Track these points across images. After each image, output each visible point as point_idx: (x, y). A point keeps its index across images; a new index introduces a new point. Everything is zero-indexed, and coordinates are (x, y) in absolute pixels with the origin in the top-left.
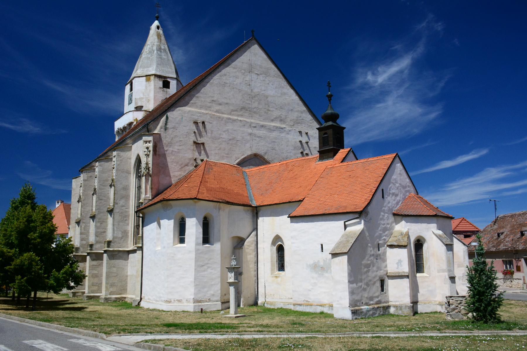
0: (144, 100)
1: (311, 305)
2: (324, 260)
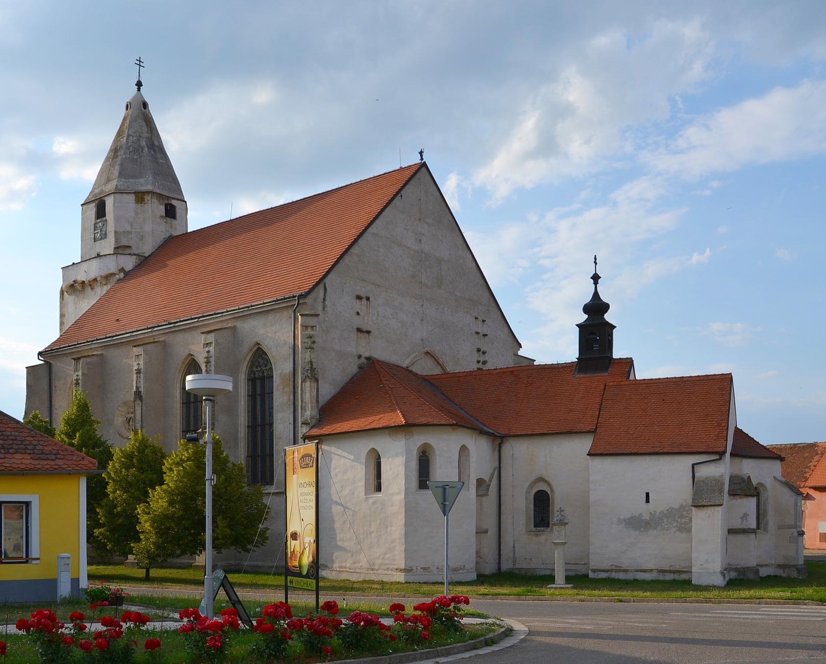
0: (133, 235)
1: (626, 571)
2: (651, 514)
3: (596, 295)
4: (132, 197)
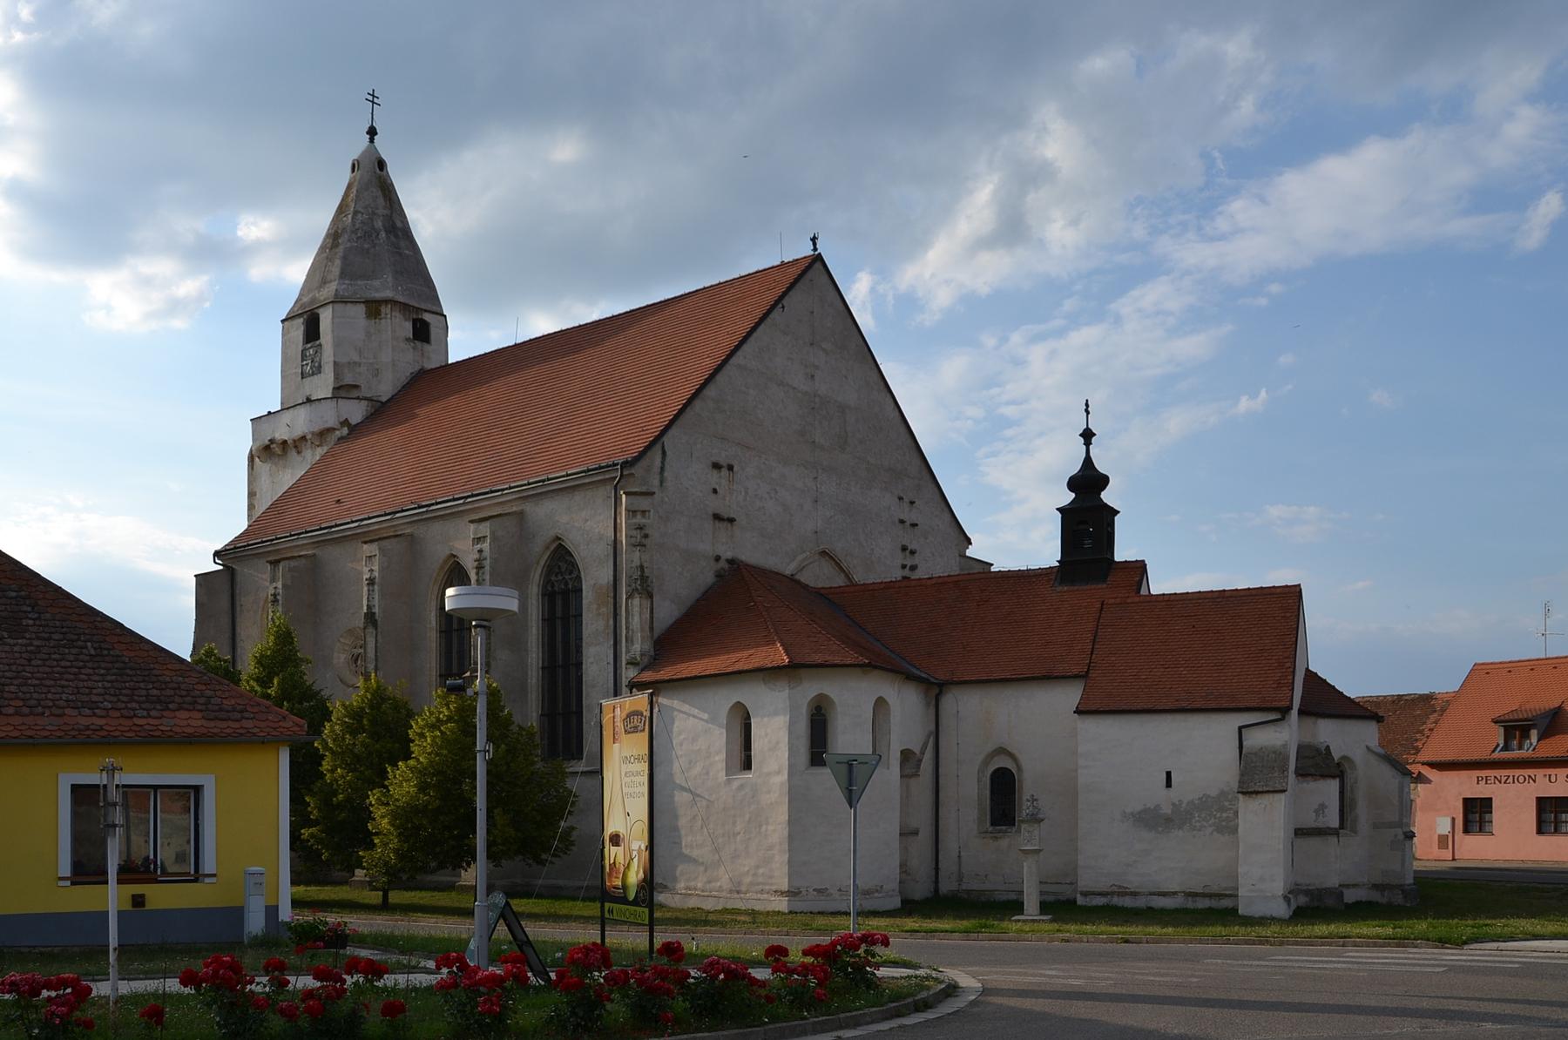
3: (1088, 462)
4: (361, 309)
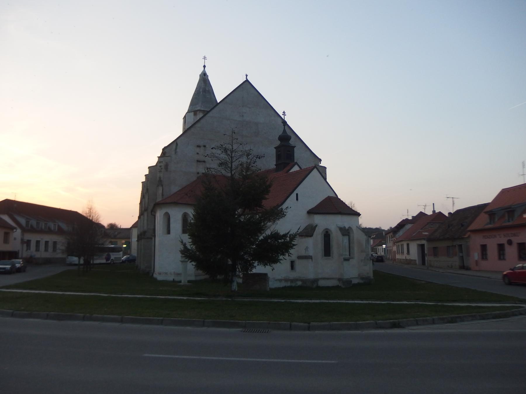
3: (284, 131)
